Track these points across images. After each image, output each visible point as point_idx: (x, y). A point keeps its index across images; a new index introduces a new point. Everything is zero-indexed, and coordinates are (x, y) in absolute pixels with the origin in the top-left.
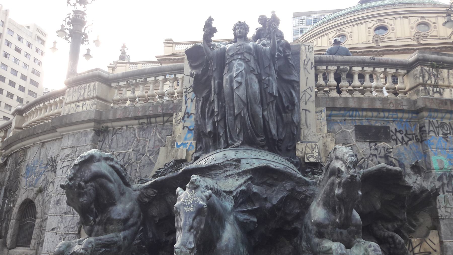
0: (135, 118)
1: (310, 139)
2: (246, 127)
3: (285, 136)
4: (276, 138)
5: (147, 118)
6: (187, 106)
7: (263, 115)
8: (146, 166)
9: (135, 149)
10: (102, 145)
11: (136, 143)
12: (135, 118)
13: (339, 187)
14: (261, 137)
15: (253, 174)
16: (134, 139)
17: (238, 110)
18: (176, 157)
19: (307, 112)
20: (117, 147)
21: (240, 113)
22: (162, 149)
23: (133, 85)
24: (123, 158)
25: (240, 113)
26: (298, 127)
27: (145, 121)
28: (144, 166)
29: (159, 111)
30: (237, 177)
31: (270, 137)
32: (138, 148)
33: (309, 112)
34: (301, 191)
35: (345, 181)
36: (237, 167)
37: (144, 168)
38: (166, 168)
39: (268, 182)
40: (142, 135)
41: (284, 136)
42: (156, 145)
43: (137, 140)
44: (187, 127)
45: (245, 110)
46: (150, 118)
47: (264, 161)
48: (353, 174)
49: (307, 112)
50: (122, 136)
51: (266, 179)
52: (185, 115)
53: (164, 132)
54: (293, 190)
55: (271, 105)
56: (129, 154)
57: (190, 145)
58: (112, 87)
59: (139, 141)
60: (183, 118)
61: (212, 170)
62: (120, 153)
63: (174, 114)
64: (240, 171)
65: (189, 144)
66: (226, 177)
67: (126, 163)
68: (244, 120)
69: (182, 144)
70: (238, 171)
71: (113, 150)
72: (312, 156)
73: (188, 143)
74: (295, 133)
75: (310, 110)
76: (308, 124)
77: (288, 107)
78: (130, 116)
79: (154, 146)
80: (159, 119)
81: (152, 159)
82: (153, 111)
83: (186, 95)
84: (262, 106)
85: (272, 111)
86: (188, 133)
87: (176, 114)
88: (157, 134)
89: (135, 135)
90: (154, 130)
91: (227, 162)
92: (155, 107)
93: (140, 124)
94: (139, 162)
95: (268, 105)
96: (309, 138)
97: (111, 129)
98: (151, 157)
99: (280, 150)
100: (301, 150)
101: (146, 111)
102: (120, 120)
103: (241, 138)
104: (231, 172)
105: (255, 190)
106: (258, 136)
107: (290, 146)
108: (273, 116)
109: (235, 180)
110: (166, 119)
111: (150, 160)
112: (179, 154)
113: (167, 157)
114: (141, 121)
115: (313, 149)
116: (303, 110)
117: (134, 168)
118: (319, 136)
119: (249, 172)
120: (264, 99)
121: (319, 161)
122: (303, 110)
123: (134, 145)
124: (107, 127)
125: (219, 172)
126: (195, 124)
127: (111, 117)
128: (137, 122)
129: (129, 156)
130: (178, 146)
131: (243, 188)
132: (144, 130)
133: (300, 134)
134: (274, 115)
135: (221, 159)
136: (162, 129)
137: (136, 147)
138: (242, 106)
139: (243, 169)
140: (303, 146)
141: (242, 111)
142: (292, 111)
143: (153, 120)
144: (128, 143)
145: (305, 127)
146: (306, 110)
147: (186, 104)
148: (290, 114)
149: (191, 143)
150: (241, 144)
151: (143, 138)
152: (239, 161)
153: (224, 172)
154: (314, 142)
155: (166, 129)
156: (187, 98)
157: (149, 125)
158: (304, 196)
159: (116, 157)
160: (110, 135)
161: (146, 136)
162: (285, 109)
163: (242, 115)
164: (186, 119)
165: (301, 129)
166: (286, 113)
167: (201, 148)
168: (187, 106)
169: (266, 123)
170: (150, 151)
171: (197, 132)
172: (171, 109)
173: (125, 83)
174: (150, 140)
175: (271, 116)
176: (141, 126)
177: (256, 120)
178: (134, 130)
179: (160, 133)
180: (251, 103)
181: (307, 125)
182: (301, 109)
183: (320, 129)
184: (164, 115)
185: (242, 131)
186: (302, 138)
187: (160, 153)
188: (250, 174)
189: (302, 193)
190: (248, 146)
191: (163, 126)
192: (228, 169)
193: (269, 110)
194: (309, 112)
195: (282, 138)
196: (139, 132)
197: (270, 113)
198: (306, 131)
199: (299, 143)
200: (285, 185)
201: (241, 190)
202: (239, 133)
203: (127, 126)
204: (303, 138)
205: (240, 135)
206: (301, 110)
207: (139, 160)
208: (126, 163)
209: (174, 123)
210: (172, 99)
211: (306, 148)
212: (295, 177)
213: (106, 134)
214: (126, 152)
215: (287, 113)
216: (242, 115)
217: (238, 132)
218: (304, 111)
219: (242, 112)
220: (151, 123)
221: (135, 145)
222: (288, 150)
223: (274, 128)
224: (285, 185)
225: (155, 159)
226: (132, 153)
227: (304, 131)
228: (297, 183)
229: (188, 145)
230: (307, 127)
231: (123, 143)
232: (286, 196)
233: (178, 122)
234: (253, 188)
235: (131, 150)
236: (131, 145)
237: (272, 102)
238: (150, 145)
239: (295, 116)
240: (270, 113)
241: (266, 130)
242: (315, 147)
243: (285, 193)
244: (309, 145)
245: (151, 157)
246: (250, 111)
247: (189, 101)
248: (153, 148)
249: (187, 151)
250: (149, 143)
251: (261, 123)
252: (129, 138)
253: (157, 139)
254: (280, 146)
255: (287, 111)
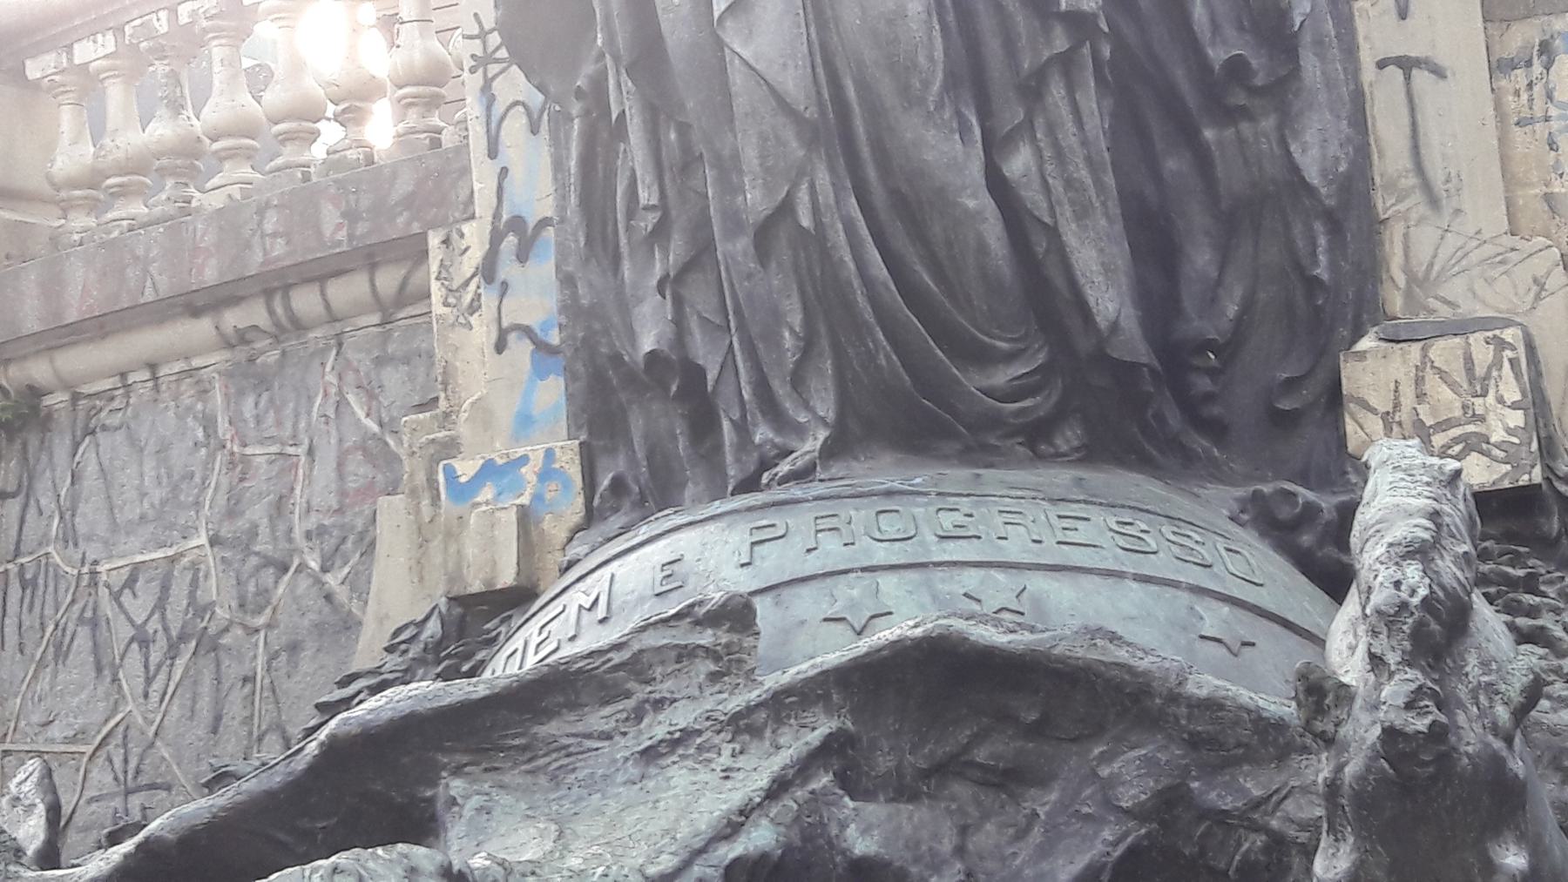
0: (194, 305)
1: (1461, 295)
2: (849, 306)
3: (1248, 306)
4: (1133, 345)
5: (268, 294)
6: (504, 172)
7: (998, 184)
8: (307, 653)
9: (225, 531)
10: (22, 521)
11: (225, 481)
12: (194, 305)
13: (1332, 829)
14: (1010, 357)
15: (856, 713)
16: (211, 457)
17: (769, 189)
18: (455, 577)
19: (1421, 77)
20: (114, 527)
21: (786, 208)
22: (392, 514)
23: (160, 53)
24: (161, 606)
25: (786, 208)
26: (1351, 212)
27: (254, 314)
28: (294, 648)
29: (328, 230)
30: (727, 750)
31: (1084, 345)
32: (242, 524)
33: (1438, 72)
34: (1229, 803)
35: (1361, 778)
36: (728, 667)
37: (293, 664)
38: (393, 661)
39: (981, 755)
40: (258, 420)
41: (1232, 310)
42: (352, 484)
43: (232, 464)
44: (527, 331)
45: (823, 178)
46: (286, 289)
47: (971, 579)
48: (1400, 719)
49: (1421, 77)
50: (133, 441)
51: (964, 736)
52: (496, 238)
53: (393, 379)
54: (1169, 803)
55: (1056, 92)
56: (194, 567)
57: (545, 475)
58: (35, 86)
59: (240, 466)
60: (488, 271)
61: (549, 714)
62: (136, 568)
63: (434, 240)
64: (753, 696)
65: (537, 459)
66: (650, 755)
67: (183, 638)
68: (826, 253)
69: (488, 471)
70: (735, 703)
71: (91, 557)
72: (1475, 444)
73: (524, 460)
74: (1322, 271)
75: (1442, 59)
76: (1437, 175)
77: (1237, 68)
78: (149, 296)
79: (343, 493)
80: (345, 291)
81: (342, 594)
82: (287, 236)
83: (487, 87)
84: (984, 114)
85: (1069, 135)
86: (540, 373)
87: (446, 242)
88: (351, 398)
89: (209, 424)
90: (331, 378)
91: (653, 639)
92: (302, 200)
93: (230, 346)
94: (261, 620)
95: (1032, 91)
96: (1455, 289)
97: (57, 400)
98: (332, 580)
99: (1217, 430)
100: (1381, 402)
101: (248, 245)
102: (99, 327)
103: (826, 406)
104: (683, 716)
105: (861, 844)
106: (983, 357)
107: (1291, 384)
108: (1084, 174)
109: (713, 778)
110: (388, 280)
111: (328, 597)
112: (471, 551)
113: (419, 568)
114: (233, 319)
115: (1479, 384)
116: (1382, 65)
117: (233, 670)
118: (1539, 265)
119: (826, 698)
120: (993, 46)
121: (1537, 475)
122: (1382, 65)
123: (214, 500)
124: (35, 393)
125: (599, 719)
126: (563, 309)
127: (31, 324)
128: (202, 328)
129: (194, 583)
130: (463, 492)
131: (761, 837)
132: (262, 382)
133: (1369, 270)
134: (1089, 160)
135: (641, 600)
136: (379, 362)
137: (232, 513)
138: (796, 150)
139: (772, 681)
140: (1400, 364)
141: (795, 186)
142: (1282, 91)
143: (306, 301)
144: (175, 489)
145: (1415, 204)
146: (1407, 64)
147: (493, 153)
148: (1268, 123)
149: (549, 454)
150: (830, 452)
151: (261, 443)
152: (736, 615)
153: (638, 715)
154: (1483, 324)
155: (406, 361)
156: (498, 109)
157: (291, 343)
158: (1260, 840)
159: (116, 597)
160: (61, 446)
161: (279, 423)
162: (1225, 91)
163: (806, 221)
164: (508, 268)
165: (1374, 227)
166: (1229, 115)
167: (618, 486)
168: (504, 172)
169: (1041, 246)
170: (322, 531)
171: (580, 368)
172: (409, 202)
173: (108, 43)
174: (311, 452)
175: (1069, 183)
176: (241, 354)
177: (937, 230)
178: (203, 393)
179: (370, 393)
180: (875, 112)
181: (1427, 186)
182: (1367, 58)
183: (1548, 198)
184: (370, 258)
185: (825, 344)
186: (1396, 302)
187: (381, 549)
188: (830, 711)
189: (1250, 815)
190: (887, 458)
191: (386, 338)
192: (664, 688)
193: (1051, 129)
194: (1438, 72)
195: (1213, 330)
196: (234, 399)
197: (1060, 156)
198: (1425, 240)
199: (1366, 343)
200: (1105, 772)
201: (736, 861)
202: (799, 364)
203: (153, 367)
204: (1409, 295)
205: (813, 383)
206: (1368, 73)
207: (259, 611)
208: (183, 638)
209: (438, 308)
210: (436, 121)
211: (1419, 381)
212: (1174, 698)
213: (34, 441)
214: (172, 560)
215: (1244, 113)
216: (806, 221)
217: (791, 360)
218: (1395, 73)
219: (803, 196)
220: (299, 325)
221: (222, 500)
222: (1284, 422)
223: (1107, 269)
224: (1105, 772)
225: (359, 584)
226: (210, 558)
227: (1411, 242)
228: (1194, 742)
229: (528, 472)
230: (1434, 202)
231: (143, 495)
232: (1123, 859)
233: (468, 298)
234: (843, 826)
235: (203, 540)
236: (197, 504)
237: (1066, 62)
238: (316, 488)
239: (1311, 136)
240: (1060, 156)
241: (1045, 294)
242: (1497, 364)
243: (1107, 834)
244: (1444, 351)
245: (332, 580)
246: (872, 173)
247: (516, 125)
248: (340, 511)
249: (526, 519)
250: (308, 476)
251: (982, 249)
252: (179, 456)
253: (352, 439)
254: (1209, 398)
255: (1239, 98)
